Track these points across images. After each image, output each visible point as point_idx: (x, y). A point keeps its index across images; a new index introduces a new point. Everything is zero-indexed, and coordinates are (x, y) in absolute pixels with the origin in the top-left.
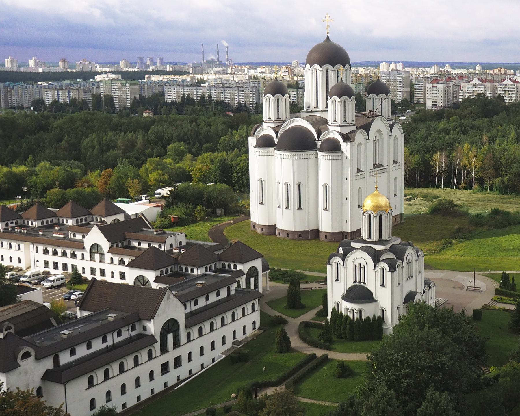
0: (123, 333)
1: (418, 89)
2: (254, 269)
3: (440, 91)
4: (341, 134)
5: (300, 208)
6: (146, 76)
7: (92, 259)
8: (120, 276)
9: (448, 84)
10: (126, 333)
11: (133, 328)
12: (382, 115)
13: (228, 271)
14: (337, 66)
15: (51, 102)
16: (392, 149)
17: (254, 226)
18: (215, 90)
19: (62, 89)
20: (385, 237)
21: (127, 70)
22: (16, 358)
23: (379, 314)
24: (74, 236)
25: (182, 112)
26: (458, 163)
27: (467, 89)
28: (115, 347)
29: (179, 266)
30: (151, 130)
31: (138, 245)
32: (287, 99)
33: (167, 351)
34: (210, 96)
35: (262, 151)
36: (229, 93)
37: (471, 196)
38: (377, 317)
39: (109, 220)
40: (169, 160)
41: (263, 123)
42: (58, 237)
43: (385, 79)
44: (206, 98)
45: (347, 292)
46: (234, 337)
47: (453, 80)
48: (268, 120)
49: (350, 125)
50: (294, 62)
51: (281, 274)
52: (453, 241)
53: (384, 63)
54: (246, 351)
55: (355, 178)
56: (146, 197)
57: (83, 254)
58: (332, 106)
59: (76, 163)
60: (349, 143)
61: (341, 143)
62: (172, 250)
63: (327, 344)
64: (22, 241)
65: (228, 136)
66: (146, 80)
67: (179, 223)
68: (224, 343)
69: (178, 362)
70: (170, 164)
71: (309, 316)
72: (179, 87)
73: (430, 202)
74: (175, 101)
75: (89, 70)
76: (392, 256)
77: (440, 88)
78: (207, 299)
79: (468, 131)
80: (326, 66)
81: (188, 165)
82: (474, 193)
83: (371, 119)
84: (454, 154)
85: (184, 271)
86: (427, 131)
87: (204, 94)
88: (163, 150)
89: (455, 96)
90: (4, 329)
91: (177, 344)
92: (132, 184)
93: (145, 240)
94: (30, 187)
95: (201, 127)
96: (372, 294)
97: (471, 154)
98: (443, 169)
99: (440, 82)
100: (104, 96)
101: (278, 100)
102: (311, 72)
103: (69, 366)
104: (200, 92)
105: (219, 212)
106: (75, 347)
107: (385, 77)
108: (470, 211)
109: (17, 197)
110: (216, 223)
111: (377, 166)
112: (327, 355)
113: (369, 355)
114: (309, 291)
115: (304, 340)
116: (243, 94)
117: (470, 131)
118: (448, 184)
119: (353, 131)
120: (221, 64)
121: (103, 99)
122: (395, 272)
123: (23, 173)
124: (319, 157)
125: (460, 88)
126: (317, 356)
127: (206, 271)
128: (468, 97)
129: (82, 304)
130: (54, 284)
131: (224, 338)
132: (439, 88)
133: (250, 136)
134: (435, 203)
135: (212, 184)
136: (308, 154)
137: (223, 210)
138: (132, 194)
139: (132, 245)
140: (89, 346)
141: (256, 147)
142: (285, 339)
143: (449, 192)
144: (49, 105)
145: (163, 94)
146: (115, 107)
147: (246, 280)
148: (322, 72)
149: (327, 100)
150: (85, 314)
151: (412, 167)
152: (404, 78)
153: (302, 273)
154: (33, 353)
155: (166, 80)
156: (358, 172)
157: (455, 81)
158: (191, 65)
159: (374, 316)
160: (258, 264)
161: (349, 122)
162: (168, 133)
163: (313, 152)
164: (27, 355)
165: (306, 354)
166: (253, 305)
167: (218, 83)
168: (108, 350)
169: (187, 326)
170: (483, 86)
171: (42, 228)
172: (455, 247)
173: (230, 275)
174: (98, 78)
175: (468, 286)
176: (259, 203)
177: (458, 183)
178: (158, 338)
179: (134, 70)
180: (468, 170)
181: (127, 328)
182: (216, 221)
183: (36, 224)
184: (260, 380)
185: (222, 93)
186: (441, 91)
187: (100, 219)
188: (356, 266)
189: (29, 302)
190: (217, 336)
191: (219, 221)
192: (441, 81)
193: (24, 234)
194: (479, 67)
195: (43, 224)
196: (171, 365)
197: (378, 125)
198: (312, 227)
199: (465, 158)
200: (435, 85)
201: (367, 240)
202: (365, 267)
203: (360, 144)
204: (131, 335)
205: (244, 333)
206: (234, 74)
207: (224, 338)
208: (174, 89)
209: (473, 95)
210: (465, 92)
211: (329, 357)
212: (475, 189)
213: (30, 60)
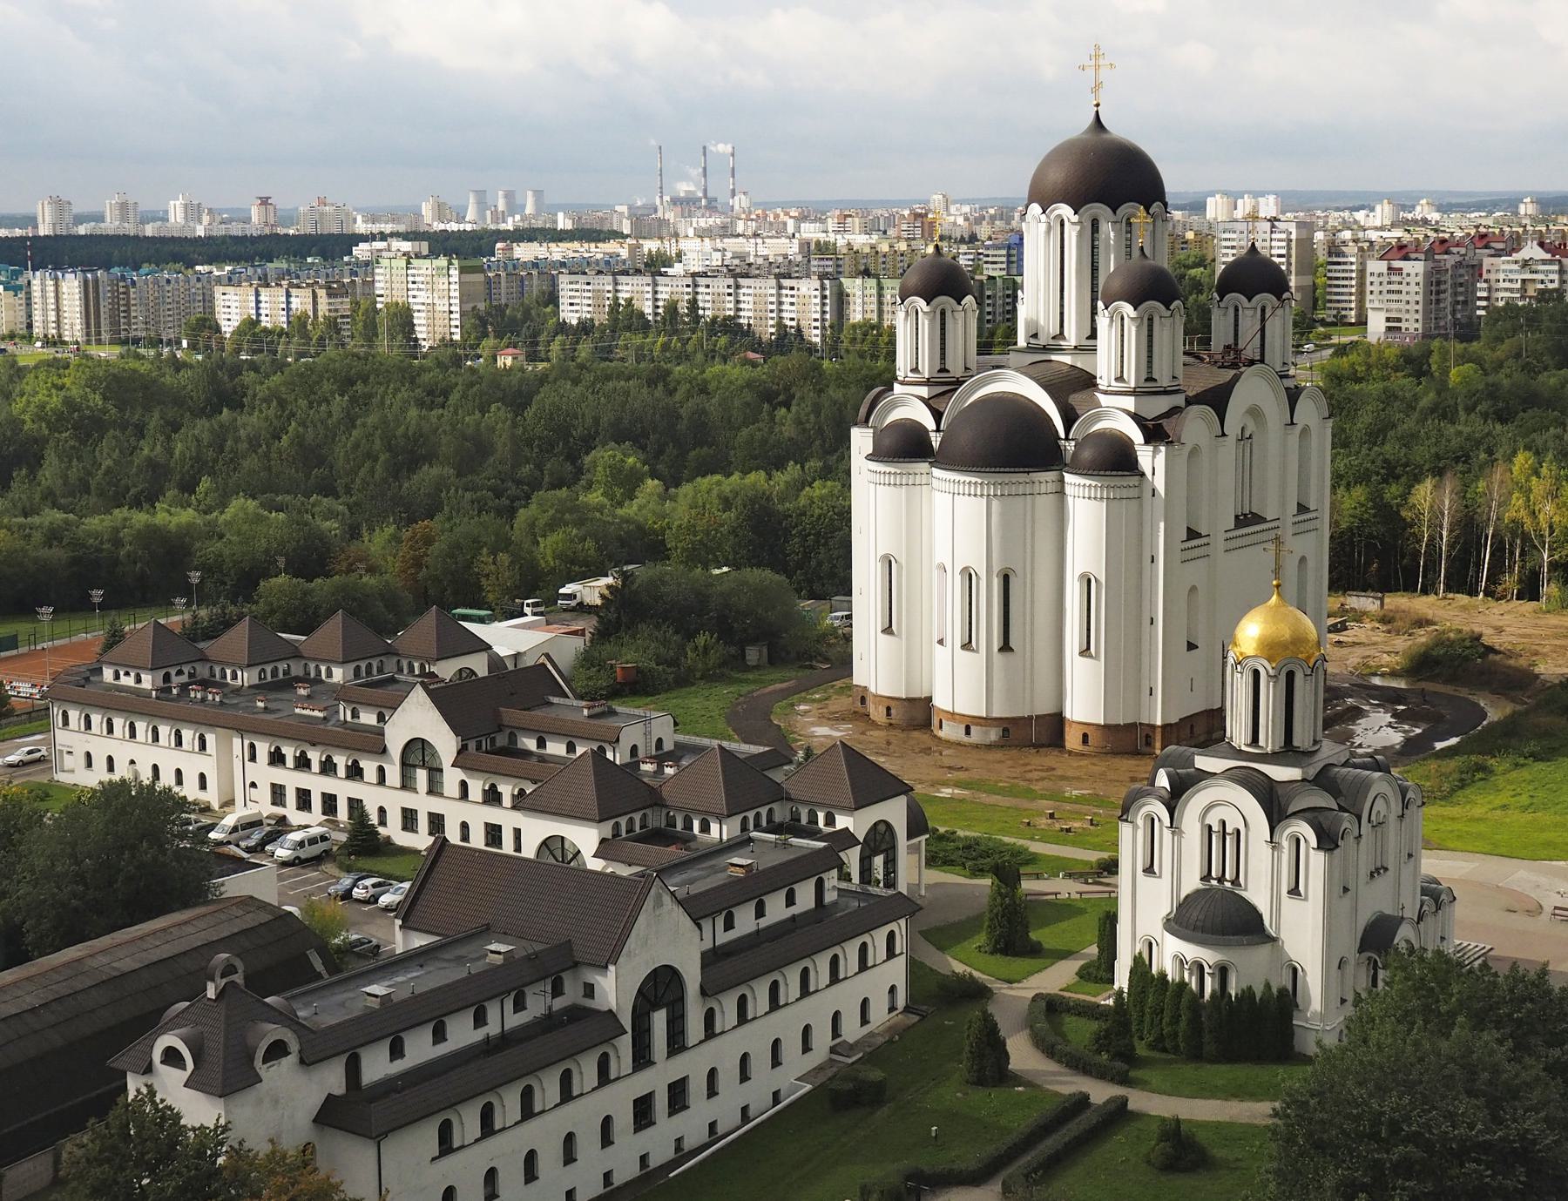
0: (530, 1000)
1: (1337, 279)
2: (882, 828)
3: (1413, 284)
4: (1136, 417)
5: (1006, 647)
6: (499, 245)
7: (407, 784)
8: (486, 837)
9: (1439, 261)
10: (538, 1004)
11: (557, 991)
12: (1262, 361)
13: (813, 833)
14: (1125, 209)
15: (237, 324)
16: (1293, 467)
17: (863, 700)
18: (708, 286)
19: (268, 286)
20: (1301, 739)
21: (442, 227)
22: (251, 1059)
23: (1283, 980)
24: (355, 715)
25: (611, 352)
26: (1493, 516)
27: (1501, 276)
28: (506, 1040)
29: (664, 812)
30: (534, 408)
31: (539, 747)
32: (970, 314)
33: (651, 1063)
34: (693, 305)
35: (893, 470)
36: (749, 295)
37: (1538, 621)
38: (1275, 991)
39: (446, 670)
40: (595, 497)
41: (896, 386)
42: (309, 716)
43: (1233, 247)
44: (681, 311)
45: (1180, 906)
46: (836, 1033)
47: (1455, 250)
48: (912, 377)
49: (1166, 393)
50: (935, 197)
51: (958, 848)
52: (1492, 761)
53: (1218, 196)
54: (876, 1075)
55: (1178, 556)
56: (535, 605)
57: (381, 770)
58: (1110, 330)
59: (326, 502)
60: (1163, 448)
61: (1137, 448)
62: (637, 764)
63: (1119, 1065)
64: (212, 725)
65: (761, 425)
66: (499, 255)
67: (638, 686)
68: (806, 1048)
69: (678, 1095)
70: (600, 508)
71: (1057, 978)
72: (601, 277)
73: (1406, 637)
74: (592, 320)
75: (335, 230)
76: (1322, 800)
77: (1413, 274)
78: (760, 913)
79: (1517, 413)
80: (1133, 207)
81: (654, 513)
82: (1549, 612)
83: (1232, 372)
84: (1482, 485)
85: (679, 826)
86: (1383, 410)
87: (675, 297)
88: (569, 467)
89: (1461, 298)
90: (218, 974)
91: (677, 1044)
92: (493, 567)
93: (557, 734)
94: (207, 569)
95: (678, 396)
96: (1260, 916)
97: (1538, 487)
98: (1445, 533)
99: (1413, 256)
100: (387, 305)
101: (943, 313)
102: (1043, 227)
103: (388, 1087)
104: (664, 293)
105: (753, 655)
106: (402, 1034)
107: (1234, 240)
108: (1541, 669)
109: (177, 600)
110: (745, 689)
111: (1246, 520)
112: (1124, 1102)
113: (1277, 1105)
114: (1048, 902)
115: (1049, 1050)
116: (793, 296)
117: (1524, 411)
118: (1462, 582)
119: (1174, 411)
120: (712, 207)
121: (383, 314)
122: (1337, 852)
123: (188, 530)
124: (1068, 489)
125: (1481, 275)
126: (1092, 1100)
127: (744, 828)
128: (1507, 303)
129: (408, 914)
130: (303, 854)
131: (807, 1030)
132: (1409, 275)
133: (856, 424)
134: (1423, 640)
135: (725, 569)
136: (1036, 480)
137: (765, 650)
138: (491, 597)
139: (519, 746)
140: (439, 1036)
141: (871, 457)
142: (991, 1045)
143: (1464, 608)
144: (233, 333)
145: (552, 299)
146: (416, 340)
147: (861, 860)
148: (1078, 228)
149: (1094, 312)
150: (419, 941)
151: (1344, 526)
152: (1293, 244)
153: (1021, 846)
154: (294, 1047)
155: (557, 257)
156: (1188, 539)
157: (1463, 251)
158: (623, 209)
159: (1268, 986)
160: (894, 812)
161: (1164, 381)
162: (583, 415)
163: (1051, 476)
164: (277, 1051)
165: (1057, 1094)
166: (891, 937)
167: (714, 263)
168: (489, 1047)
169: (707, 991)
170: (1556, 268)
171: (261, 688)
172: (1500, 781)
173: (823, 844)
174: (362, 251)
175: (1556, 908)
176: (879, 630)
177: (1493, 578)
178: (626, 1021)
179: (461, 227)
180: (1526, 538)
181: (539, 987)
182: (747, 681)
183: (246, 678)
184: (927, 1161)
185: (730, 294)
186: (1417, 284)
187: (422, 667)
188: (1210, 827)
189: (249, 902)
190: (786, 1025)
191: (755, 682)
192: (1416, 251)
193: (213, 704)
194: (1530, 206)
195: (277, 676)
196: (661, 1103)
197: (1252, 390)
198: (1044, 707)
199: (1517, 500)
200: (1397, 264)
201: (1244, 748)
202: (1238, 832)
203: (1195, 451)
204: (550, 1008)
205: (865, 1021)
206: (756, 235)
207: (807, 1030)
208: (588, 284)
209: (1523, 297)
210: (1496, 286)
211: (1131, 1106)
212: (1548, 599)
213: (172, 203)
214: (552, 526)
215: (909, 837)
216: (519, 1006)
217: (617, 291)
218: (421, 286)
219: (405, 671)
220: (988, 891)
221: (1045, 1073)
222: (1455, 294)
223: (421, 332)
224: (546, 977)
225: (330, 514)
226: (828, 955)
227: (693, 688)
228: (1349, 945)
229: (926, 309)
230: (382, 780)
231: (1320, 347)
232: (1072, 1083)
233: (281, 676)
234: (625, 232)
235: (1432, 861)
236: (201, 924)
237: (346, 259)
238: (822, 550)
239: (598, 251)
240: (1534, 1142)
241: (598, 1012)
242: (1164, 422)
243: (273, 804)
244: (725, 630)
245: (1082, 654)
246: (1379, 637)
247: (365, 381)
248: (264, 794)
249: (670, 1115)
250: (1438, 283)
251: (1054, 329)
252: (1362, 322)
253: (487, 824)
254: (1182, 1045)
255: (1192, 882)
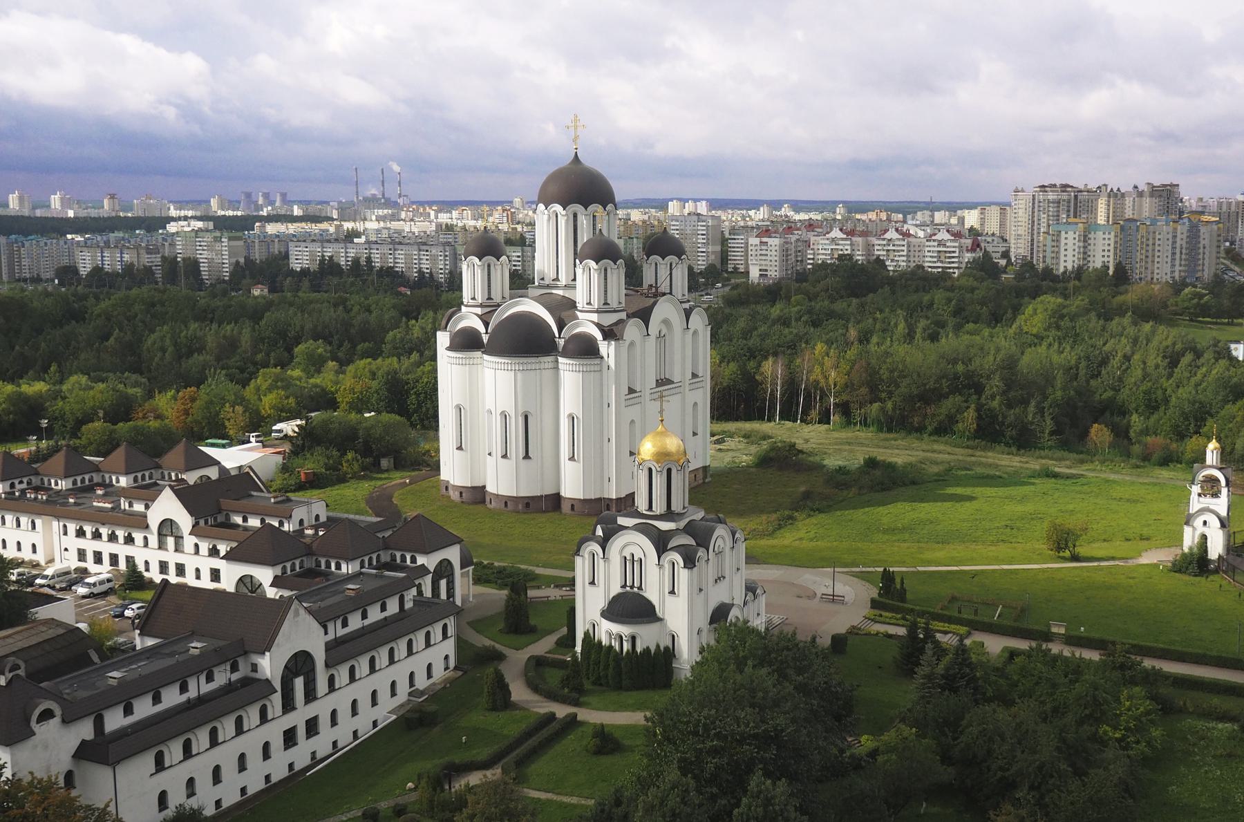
1: (734, 247)
2: (445, 563)
3: (773, 251)
4: (598, 325)
6: (257, 224)
7: (162, 546)
10: (222, 677)
11: (234, 668)
14: (592, 207)
15: (89, 270)
16: (689, 353)
17: (447, 488)
18: (378, 249)
19: (109, 247)
20: (676, 506)
21: (223, 213)
22: (28, 721)
25: (320, 287)
26: (804, 377)
27: (820, 247)
28: (201, 700)
29: (314, 558)
30: (265, 319)
32: (505, 266)
33: (294, 708)
34: (369, 260)
38: (662, 649)
39: (192, 477)
40: (297, 373)
41: (463, 307)
43: (677, 230)
44: (362, 263)
45: (610, 603)
46: (412, 684)
47: (796, 232)
49: (615, 311)
52: (796, 514)
53: (675, 201)
54: (432, 708)
55: (623, 403)
56: (257, 436)
57: (146, 538)
59: (134, 377)
60: (613, 343)
61: (599, 342)
62: (303, 530)
63: (574, 695)
64: (39, 514)
66: (257, 231)
67: (314, 483)
68: (393, 694)
69: (312, 727)
70: (300, 379)
71: (543, 646)
74: (308, 268)
75: (157, 214)
78: (364, 616)
83: (652, 300)
84: (798, 361)
85: (323, 567)
87: (359, 255)
88: (286, 354)
89: (799, 259)
91: (310, 696)
92: (232, 414)
93: (255, 513)
94: (52, 420)
95: (352, 314)
96: (654, 607)
97: (828, 362)
99: (774, 235)
100: (184, 259)
101: (489, 266)
102: (546, 217)
103: (122, 734)
104: (352, 253)
105: (385, 463)
109: (30, 437)
110: (379, 483)
111: (662, 382)
112: (575, 715)
118: (788, 415)
119: (620, 322)
121: (181, 265)
122: (695, 569)
124: (560, 366)
125: (809, 246)
126: (557, 716)
127: (362, 566)
129: (145, 625)
130: (96, 590)
131: (393, 684)
135: (373, 413)
136: (542, 361)
137: (392, 460)
138: (231, 432)
139: (232, 521)
140: (157, 699)
142: (501, 687)
143: (789, 429)
144: (87, 275)
147: (433, 583)
149: (575, 266)
150: (150, 642)
151: (725, 384)
153: (531, 570)
154: (58, 712)
155: (291, 231)
157: (800, 233)
159: (658, 646)
160: (453, 554)
161: (614, 304)
162: (295, 324)
164: (47, 715)
166: (445, 627)
168: (190, 705)
170: (849, 242)
171: (74, 491)
174: (172, 228)
175: (823, 594)
176: (455, 448)
178: (278, 685)
180: (822, 390)
181: (222, 667)
182: (381, 479)
183: (63, 485)
184: (458, 758)
185: (391, 254)
187: (177, 475)
188: (625, 558)
190: (380, 682)
191: (385, 479)
193: (42, 502)
196: (301, 732)
197: (664, 310)
198: (549, 491)
199: (817, 369)
200: (765, 240)
201: (644, 512)
202: (641, 560)
203: (632, 344)
204: (230, 679)
205: (429, 676)
206: (412, 220)
207: (393, 684)
211: (579, 718)
213: (52, 196)
214: (270, 389)
215: (462, 568)
216: (210, 679)
217: (347, 252)
218: (205, 248)
219: (167, 478)
220: (506, 598)
221: (528, 702)
222: (797, 256)
223: (205, 275)
224: (227, 661)
225: (136, 384)
226: (405, 640)
227: (347, 484)
228: (703, 620)
229: (479, 263)
230: (146, 545)
231: (723, 286)
232: (548, 707)
233: (87, 482)
234: (335, 217)
235: (759, 570)
236: (18, 637)
237: (160, 231)
238: (429, 402)
239: (315, 228)
240: (782, 731)
241: (259, 680)
242: (614, 328)
243: (79, 560)
244: (366, 450)
245: (569, 459)
246: (741, 446)
247: (163, 305)
248: (73, 555)
249: (307, 738)
250: (787, 250)
251: (553, 276)
252: (747, 273)
253: (211, 569)
254: (610, 682)
255: (616, 589)
